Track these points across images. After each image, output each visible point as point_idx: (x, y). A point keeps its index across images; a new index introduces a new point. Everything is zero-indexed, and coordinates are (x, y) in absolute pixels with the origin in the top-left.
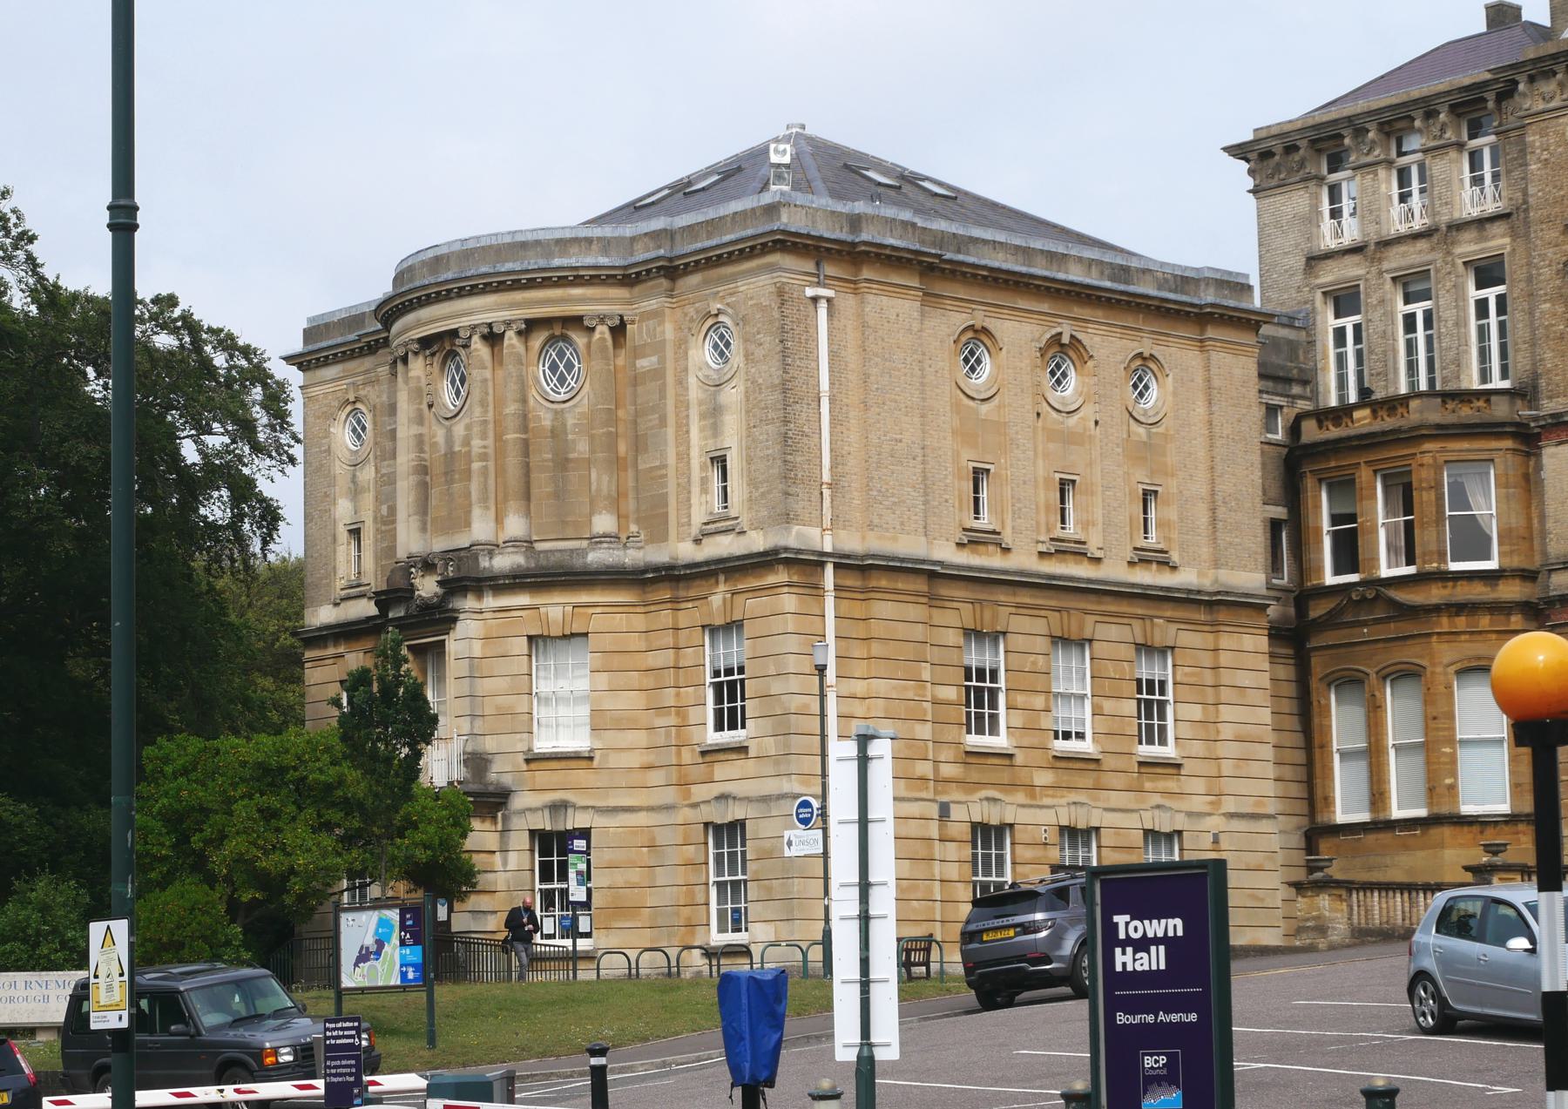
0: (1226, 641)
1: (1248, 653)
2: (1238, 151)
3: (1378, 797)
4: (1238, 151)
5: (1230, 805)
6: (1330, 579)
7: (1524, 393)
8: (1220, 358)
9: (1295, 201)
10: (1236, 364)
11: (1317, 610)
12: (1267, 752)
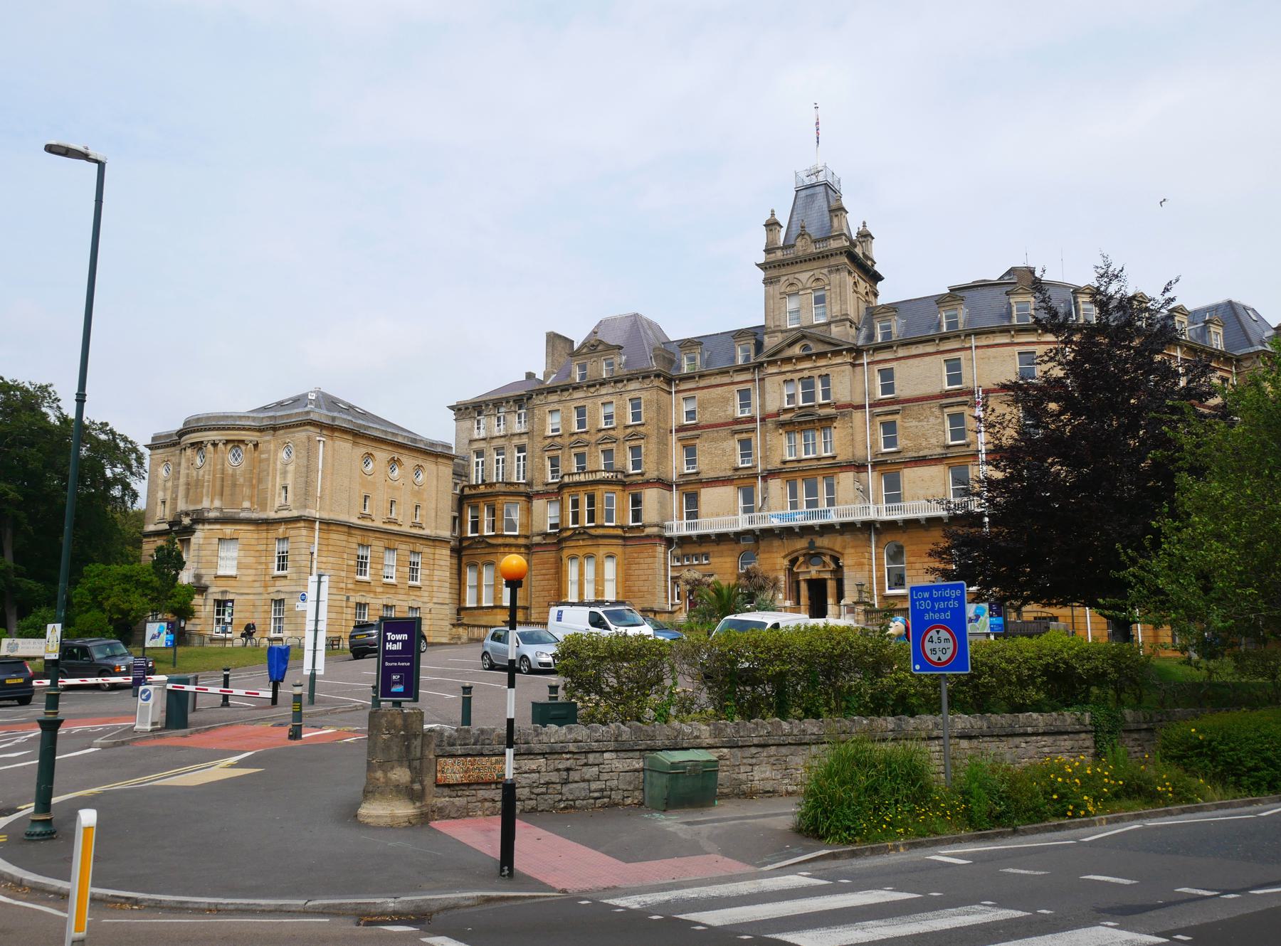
0: (437, 551)
1: (444, 554)
2: (452, 408)
3: (479, 599)
4: (452, 408)
5: (435, 600)
6: (470, 535)
7: (529, 484)
8: (441, 468)
9: (467, 424)
10: (446, 470)
11: (465, 544)
12: (447, 585)
